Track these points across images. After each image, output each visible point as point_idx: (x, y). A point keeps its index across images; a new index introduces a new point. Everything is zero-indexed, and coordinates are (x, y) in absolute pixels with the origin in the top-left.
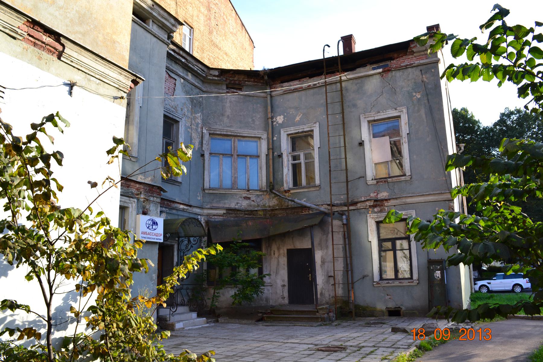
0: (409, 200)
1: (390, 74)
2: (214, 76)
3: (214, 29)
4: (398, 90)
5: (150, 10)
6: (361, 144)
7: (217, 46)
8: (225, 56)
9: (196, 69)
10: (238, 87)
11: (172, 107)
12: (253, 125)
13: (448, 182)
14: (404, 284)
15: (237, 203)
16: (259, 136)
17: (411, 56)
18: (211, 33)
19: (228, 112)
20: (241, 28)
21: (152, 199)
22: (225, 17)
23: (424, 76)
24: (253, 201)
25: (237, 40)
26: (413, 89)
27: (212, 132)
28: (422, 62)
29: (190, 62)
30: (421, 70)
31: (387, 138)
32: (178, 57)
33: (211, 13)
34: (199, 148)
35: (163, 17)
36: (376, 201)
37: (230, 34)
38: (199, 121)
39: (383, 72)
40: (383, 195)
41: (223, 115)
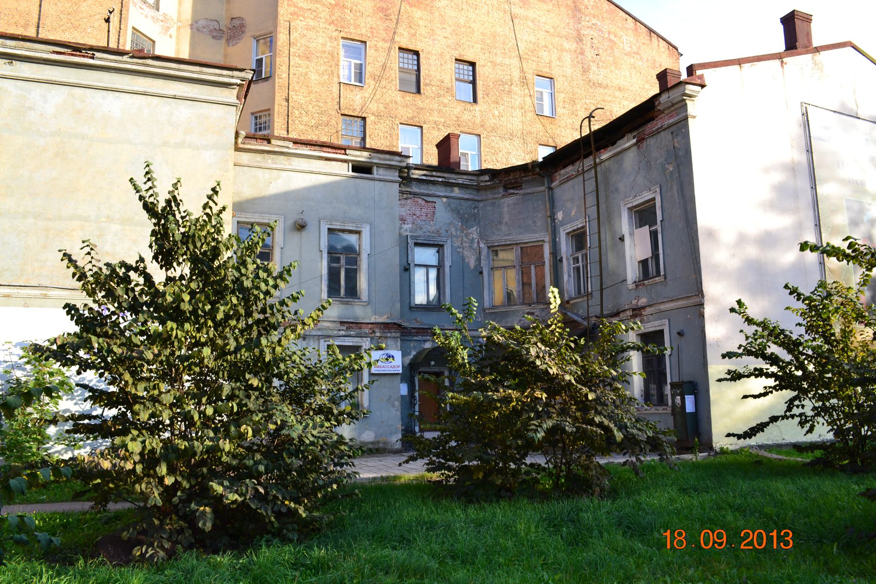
0: (663, 307)
1: (645, 144)
2: (486, 181)
3: (591, 63)
4: (652, 163)
5: (368, 160)
6: (622, 239)
7: (600, 85)
8: (617, 93)
9: (461, 182)
10: (517, 186)
11: (433, 232)
12: (534, 228)
13: (699, 282)
14: (660, 412)
15: (520, 320)
16: (542, 239)
17: (663, 115)
18: (585, 71)
19: (506, 218)
20: (648, 38)
21: (389, 335)
22: (612, 37)
23: (675, 140)
24: (537, 316)
25: (641, 59)
26: (666, 160)
27: (489, 245)
28: (671, 121)
29: (449, 178)
30: (672, 133)
31: (647, 227)
32: (432, 179)
33: (584, 42)
34: (475, 266)
35: (385, 160)
36: (633, 310)
37: (626, 58)
38: (474, 236)
39: (637, 142)
40: (643, 301)
41: (500, 223)
